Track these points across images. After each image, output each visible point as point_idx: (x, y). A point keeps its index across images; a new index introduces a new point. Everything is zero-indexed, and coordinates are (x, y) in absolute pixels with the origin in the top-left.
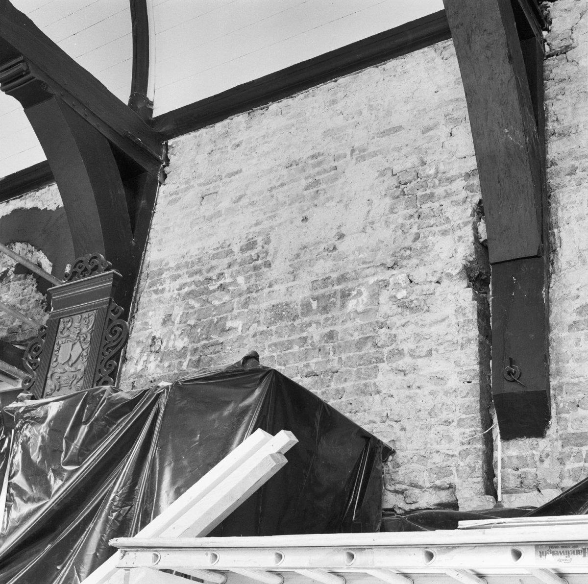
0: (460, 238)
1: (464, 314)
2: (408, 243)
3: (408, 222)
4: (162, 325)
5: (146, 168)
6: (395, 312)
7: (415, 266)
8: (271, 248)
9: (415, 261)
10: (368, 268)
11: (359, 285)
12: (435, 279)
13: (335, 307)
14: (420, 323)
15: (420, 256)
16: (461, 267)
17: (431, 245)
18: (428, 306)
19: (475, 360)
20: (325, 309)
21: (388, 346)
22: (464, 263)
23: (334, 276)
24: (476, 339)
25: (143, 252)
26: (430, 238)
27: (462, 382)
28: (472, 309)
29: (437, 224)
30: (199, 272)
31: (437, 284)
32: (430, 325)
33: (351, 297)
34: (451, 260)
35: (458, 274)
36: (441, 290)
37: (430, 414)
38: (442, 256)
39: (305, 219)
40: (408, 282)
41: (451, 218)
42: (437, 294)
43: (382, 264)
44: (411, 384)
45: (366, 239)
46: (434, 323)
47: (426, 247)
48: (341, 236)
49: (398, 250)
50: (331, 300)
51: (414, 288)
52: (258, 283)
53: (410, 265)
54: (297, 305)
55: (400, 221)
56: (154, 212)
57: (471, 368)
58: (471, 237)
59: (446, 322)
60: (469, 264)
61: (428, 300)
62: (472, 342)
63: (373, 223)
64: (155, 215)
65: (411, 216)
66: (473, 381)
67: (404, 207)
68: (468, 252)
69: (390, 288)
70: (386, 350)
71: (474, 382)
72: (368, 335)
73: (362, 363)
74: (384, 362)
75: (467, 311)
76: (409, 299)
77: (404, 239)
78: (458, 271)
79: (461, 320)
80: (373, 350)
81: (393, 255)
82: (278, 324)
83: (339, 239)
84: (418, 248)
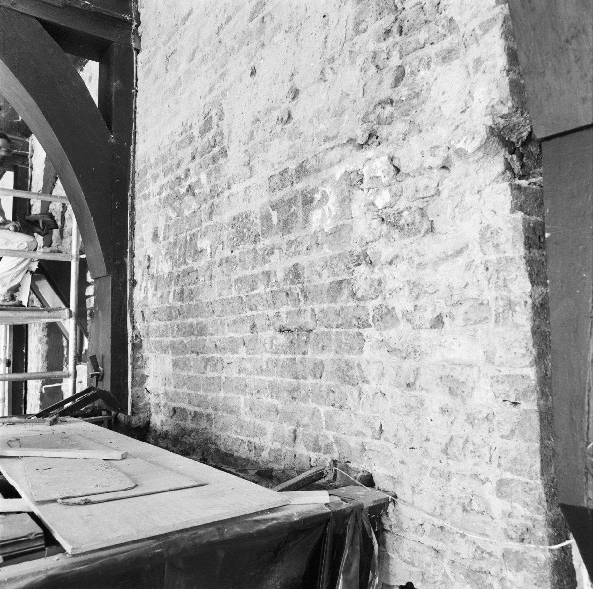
0: (478, 62)
1: (496, 246)
2: (385, 92)
3: (384, 45)
4: (153, 241)
5: (111, 39)
6: (377, 233)
7: (401, 136)
8: (224, 125)
9: (400, 127)
10: (332, 148)
11: (323, 182)
12: (439, 162)
13: (297, 222)
14: (417, 260)
15: (407, 115)
16: (483, 133)
17: (425, 87)
18: (431, 219)
19: (524, 356)
20: (286, 225)
21: (372, 299)
22: (490, 123)
23: (292, 166)
24: (526, 302)
25: (132, 147)
26: (422, 73)
27: (500, 400)
28: (511, 233)
29: (433, 39)
30: (169, 170)
31: (443, 171)
32: (436, 264)
33: (315, 203)
34: (466, 116)
35: (479, 149)
36: (452, 184)
37: (445, 452)
38: (447, 111)
39: (253, 73)
40: (392, 171)
41: (457, 19)
42: (445, 193)
43: (351, 140)
44: (412, 380)
45: (325, 94)
46: (442, 260)
47: (417, 94)
48: (295, 94)
49: (371, 108)
50: (292, 210)
51: (403, 184)
52: (218, 182)
53: (394, 135)
54: (257, 218)
55: (371, 46)
56: (137, 91)
57: (518, 371)
58: (501, 56)
59: (461, 260)
60: (502, 121)
61: (430, 207)
62: (517, 308)
63: (332, 60)
64: (139, 94)
65: (388, 32)
66: (522, 402)
67: (375, 15)
68: (496, 96)
69: (365, 185)
70: (370, 305)
71: (524, 406)
72: (340, 278)
73: (340, 322)
74: (370, 326)
75: (502, 239)
76: (396, 208)
77: (379, 84)
78: (477, 143)
79: (493, 257)
80: (352, 304)
81: (365, 120)
82: (241, 247)
83: (293, 98)
84: (403, 99)
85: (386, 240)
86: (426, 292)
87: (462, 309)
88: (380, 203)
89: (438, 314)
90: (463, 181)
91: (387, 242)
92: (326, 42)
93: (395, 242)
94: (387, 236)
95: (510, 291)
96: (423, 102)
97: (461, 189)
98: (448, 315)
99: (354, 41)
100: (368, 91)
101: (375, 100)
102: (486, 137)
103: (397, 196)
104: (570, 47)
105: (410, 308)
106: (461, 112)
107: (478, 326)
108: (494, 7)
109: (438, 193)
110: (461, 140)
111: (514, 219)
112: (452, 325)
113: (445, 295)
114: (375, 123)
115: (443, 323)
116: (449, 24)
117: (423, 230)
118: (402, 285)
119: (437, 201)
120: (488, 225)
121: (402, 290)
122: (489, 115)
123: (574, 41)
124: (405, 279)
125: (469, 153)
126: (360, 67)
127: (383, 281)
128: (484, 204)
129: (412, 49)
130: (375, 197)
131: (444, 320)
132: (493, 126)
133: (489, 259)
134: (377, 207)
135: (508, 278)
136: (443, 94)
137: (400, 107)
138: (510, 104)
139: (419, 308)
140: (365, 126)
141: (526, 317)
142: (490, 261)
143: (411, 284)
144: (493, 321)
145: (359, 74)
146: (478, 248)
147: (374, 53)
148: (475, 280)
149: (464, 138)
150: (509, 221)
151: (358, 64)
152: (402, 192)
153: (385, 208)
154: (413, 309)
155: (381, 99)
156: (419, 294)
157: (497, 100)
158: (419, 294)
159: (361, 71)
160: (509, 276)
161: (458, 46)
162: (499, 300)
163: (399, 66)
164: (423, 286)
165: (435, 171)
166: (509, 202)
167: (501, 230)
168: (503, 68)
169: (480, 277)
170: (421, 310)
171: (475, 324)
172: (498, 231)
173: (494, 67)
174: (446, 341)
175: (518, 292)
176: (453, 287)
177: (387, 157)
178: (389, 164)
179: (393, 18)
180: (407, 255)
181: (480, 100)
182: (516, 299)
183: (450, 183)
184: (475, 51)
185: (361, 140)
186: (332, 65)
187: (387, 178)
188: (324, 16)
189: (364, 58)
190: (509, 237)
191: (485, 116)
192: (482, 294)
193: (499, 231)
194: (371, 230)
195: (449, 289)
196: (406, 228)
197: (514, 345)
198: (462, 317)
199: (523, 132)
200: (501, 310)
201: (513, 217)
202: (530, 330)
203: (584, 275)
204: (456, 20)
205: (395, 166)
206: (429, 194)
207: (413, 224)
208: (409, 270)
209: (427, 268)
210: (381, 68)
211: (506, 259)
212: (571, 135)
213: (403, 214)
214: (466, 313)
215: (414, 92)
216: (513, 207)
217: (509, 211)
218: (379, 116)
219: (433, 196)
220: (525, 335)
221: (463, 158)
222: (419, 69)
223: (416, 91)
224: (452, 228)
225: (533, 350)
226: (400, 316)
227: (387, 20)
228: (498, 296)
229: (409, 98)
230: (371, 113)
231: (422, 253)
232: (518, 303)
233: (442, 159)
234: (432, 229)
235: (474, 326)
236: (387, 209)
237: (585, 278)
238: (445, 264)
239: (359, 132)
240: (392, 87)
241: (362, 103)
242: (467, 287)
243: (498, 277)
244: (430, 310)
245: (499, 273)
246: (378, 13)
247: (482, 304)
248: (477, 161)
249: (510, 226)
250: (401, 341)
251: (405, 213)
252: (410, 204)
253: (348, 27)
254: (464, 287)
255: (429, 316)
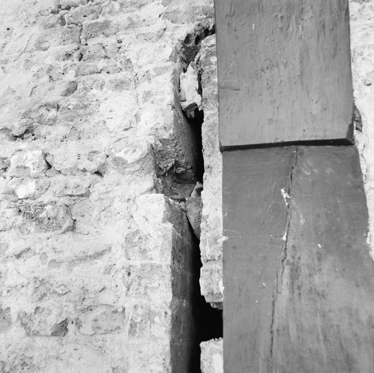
2: (55, 96)
3: (62, 64)
6: (9, 223)
7: (60, 138)
9: (61, 129)
12: (94, 166)
14: (51, 256)
15: (72, 121)
16: (145, 148)
17: (94, 103)
18: (74, 218)
22: (152, 142)
24: (166, 313)
26: (94, 91)
28: (160, 241)
29: (110, 69)
31: (96, 176)
35: (138, 161)
38: (111, 125)
40: (43, 166)
41: (134, 61)
42: (94, 196)
47: (86, 107)
49: (36, 107)
51: (52, 180)
53: (53, 136)
55: (49, 61)
58: (169, 94)
59: (101, 263)
61: (75, 206)
62: (157, 319)
68: (161, 122)
76: (39, 200)
81: (26, 115)
84: (71, 107)
85: (18, 230)
86: (55, 292)
87: (92, 316)
88: (21, 192)
89: (63, 320)
90: (114, 188)
91: (20, 233)
92: (4, 47)
93: (29, 235)
94: (20, 228)
95: (150, 300)
96: (90, 114)
97: (111, 195)
98: (74, 322)
99: (33, 54)
100: (37, 93)
101: (42, 101)
102: (147, 152)
103: (42, 190)
104: (264, 75)
105: (30, 309)
106: (125, 130)
107: (109, 336)
108: (167, 61)
109: (87, 195)
110: (122, 150)
111: (165, 228)
112: (78, 333)
113: (77, 299)
114: (36, 121)
115: (67, 330)
116: (126, 63)
117: (65, 227)
118: (26, 281)
119: (84, 202)
120: (137, 231)
121: (24, 288)
122: (153, 135)
123: (267, 71)
124: (32, 276)
125: (128, 162)
126: (34, 73)
127: (3, 275)
128: (137, 210)
129: (89, 72)
130: (17, 185)
131: (68, 327)
132: (154, 145)
133: (133, 264)
134: (17, 196)
135: (149, 286)
136: (111, 111)
137: (66, 113)
138: (171, 131)
139: (41, 310)
140: (25, 120)
141: (164, 329)
142: (134, 267)
143: (38, 282)
144: (127, 331)
145: (31, 78)
146: (121, 252)
147: (51, 66)
148: (114, 284)
149: (126, 150)
150: (160, 230)
151: (32, 70)
152: (49, 186)
153: (27, 198)
154: (33, 311)
155: (48, 102)
156: (45, 294)
157: (162, 125)
158: (45, 294)
159: (34, 76)
160: (151, 283)
161: (129, 82)
162: (139, 308)
163: (73, 82)
164: (52, 285)
165: (88, 174)
166: (163, 211)
167: (150, 237)
168: (170, 103)
169: (119, 282)
170: (43, 313)
171: (105, 334)
172: (147, 237)
173: (162, 100)
174: (65, 352)
175: (159, 302)
176: (87, 290)
177: (41, 152)
178: (42, 158)
179: (75, 46)
180: (41, 249)
181: (146, 121)
182: (157, 309)
183: (101, 188)
184: (145, 86)
185: (16, 132)
186: (4, 65)
187: (36, 171)
188: (8, 29)
189: (40, 67)
190: (158, 245)
191: (149, 135)
192: (117, 300)
193: (148, 237)
194: (3, 219)
195: (82, 292)
196: (46, 221)
197: (151, 360)
198: (90, 325)
199: (169, 163)
200: (139, 320)
201: (164, 226)
202: (169, 344)
203: (264, 284)
204: (133, 62)
205: (46, 161)
206: (79, 193)
207: (55, 218)
208: (39, 266)
209: (61, 266)
210: (54, 79)
211: (152, 266)
212: (251, 150)
213: (45, 207)
214: (96, 320)
215: (83, 104)
216: (165, 217)
217: (161, 220)
218: (41, 116)
219: (82, 196)
220: (164, 349)
221: (120, 167)
222: (92, 87)
223: (85, 103)
224: (95, 230)
225: (170, 368)
226: (14, 317)
227: (70, 47)
228: (138, 303)
229: (76, 107)
230: (34, 111)
231: (59, 249)
232: (158, 314)
233: (98, 164)
234: (73, 228)
235: (104, 336)
236: (29, 199)
237: (264, 287)
238: (81, 264)
239: (16, 124)
240: (62, 95)
241: (28, 100)
242: (103, 291)
243: (139, 284)
244: (55, 312)
245: (141, 280)
246: (62, 40)
247: (116, 312)
248: (133, 173)
249: (160, 233)
250: (9, 349)
251: (48, 208)
252: (56, 199)
253: (29, 42)
254: (100, 291)
255: (53, 320)
